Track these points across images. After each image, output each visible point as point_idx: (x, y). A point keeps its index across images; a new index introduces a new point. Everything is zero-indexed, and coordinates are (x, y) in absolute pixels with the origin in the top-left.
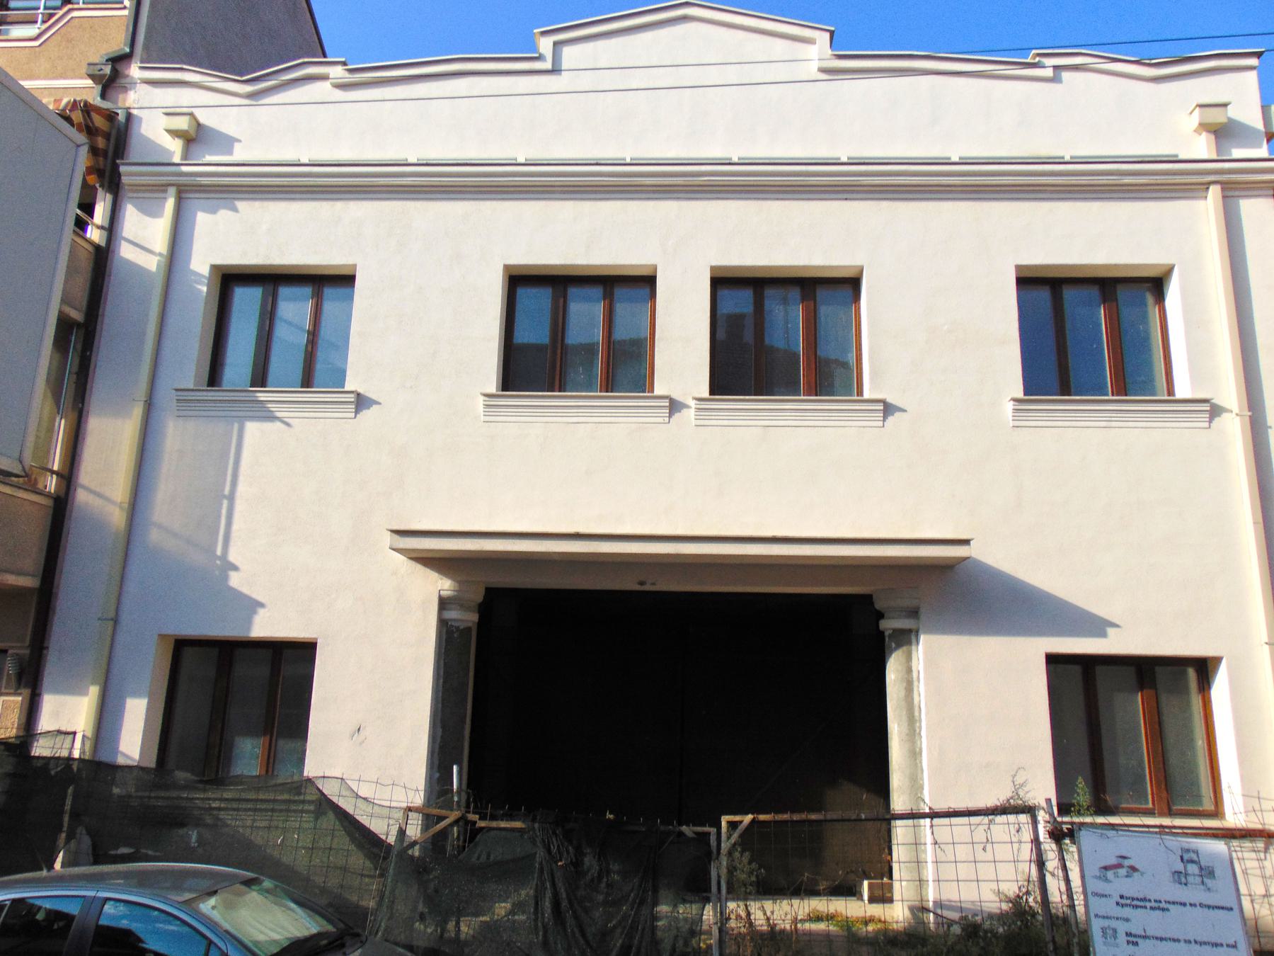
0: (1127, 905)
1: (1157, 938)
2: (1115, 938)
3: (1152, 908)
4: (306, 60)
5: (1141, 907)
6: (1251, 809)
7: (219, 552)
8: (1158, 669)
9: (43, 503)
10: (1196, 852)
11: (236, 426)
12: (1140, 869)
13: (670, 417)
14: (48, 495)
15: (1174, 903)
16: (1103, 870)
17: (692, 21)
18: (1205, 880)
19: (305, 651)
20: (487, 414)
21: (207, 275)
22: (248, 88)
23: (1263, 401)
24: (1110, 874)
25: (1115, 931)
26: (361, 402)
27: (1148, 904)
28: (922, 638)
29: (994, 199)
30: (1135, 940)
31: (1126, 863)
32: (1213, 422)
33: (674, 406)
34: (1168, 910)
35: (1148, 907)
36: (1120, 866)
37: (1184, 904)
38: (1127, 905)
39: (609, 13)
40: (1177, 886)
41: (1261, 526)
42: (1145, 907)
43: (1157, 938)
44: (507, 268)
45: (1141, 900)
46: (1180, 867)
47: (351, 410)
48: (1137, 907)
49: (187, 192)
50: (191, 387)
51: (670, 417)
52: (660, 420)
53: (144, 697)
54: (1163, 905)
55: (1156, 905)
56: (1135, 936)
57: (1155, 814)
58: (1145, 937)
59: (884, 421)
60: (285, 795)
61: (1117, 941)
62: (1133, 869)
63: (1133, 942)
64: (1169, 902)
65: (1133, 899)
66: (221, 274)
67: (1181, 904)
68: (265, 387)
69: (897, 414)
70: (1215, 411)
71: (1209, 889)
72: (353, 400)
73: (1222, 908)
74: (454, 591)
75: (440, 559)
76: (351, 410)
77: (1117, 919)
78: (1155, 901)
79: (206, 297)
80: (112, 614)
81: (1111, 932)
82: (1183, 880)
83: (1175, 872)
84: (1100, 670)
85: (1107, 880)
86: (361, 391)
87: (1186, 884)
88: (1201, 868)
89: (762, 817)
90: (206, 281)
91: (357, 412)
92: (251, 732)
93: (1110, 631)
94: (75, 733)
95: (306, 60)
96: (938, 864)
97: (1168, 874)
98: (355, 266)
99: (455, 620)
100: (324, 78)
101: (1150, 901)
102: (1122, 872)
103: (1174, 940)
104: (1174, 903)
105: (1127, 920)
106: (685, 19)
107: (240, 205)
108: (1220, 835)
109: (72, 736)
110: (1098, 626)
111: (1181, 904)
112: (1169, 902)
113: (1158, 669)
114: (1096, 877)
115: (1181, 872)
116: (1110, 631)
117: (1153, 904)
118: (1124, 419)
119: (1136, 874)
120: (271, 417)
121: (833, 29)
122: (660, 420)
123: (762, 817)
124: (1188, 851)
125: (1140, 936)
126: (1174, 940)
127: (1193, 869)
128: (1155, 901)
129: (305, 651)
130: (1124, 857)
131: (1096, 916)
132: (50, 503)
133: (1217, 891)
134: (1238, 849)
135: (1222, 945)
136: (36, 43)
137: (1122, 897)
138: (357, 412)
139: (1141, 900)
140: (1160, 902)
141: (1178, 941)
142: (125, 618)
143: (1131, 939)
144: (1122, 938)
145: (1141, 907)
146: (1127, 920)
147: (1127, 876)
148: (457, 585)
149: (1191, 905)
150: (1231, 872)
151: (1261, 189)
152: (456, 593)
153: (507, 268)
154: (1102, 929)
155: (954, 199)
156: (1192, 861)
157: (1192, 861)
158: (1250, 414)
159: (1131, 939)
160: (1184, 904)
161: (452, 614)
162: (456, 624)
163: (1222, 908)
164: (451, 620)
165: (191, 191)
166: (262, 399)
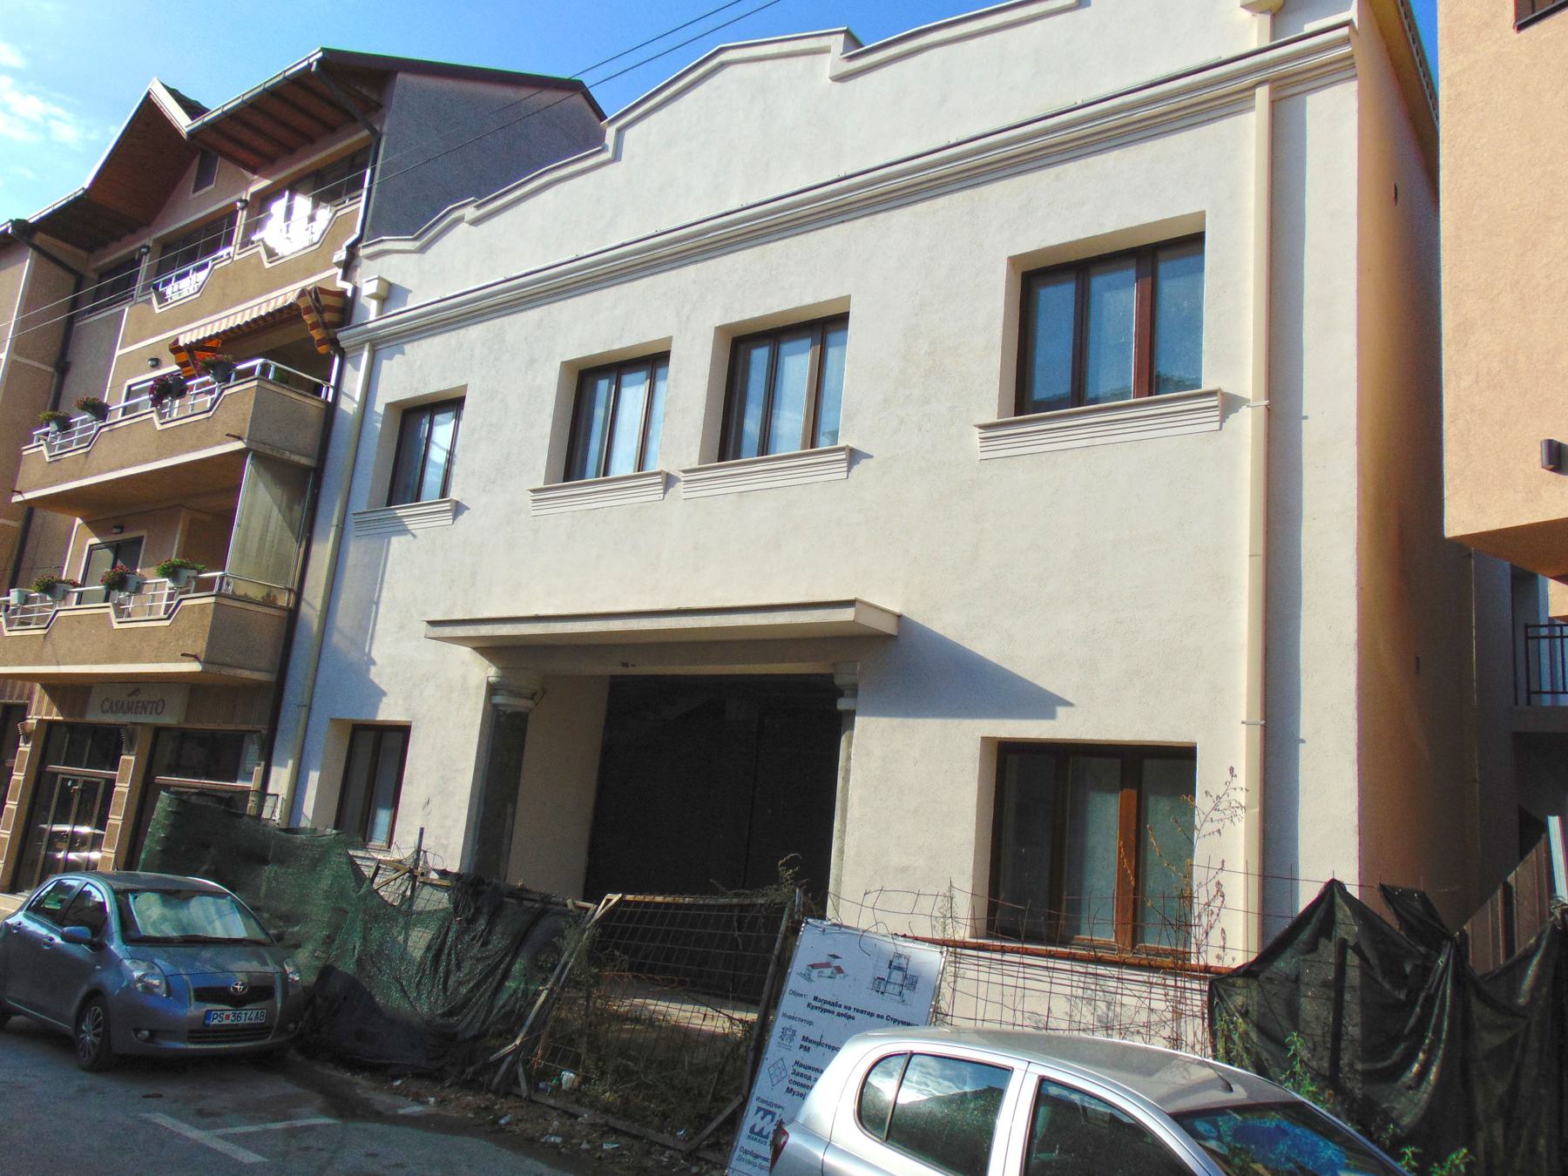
2: (791, 1040)
3: (839, 1014)
4: (451, 207)
5: (829, 1012)
7: (367, 650)
8: (1148, 763)
9: (276, 614)
10: (907, 958)
11: (386, 540)
12: (845, 971)
13: (665, 493)
14: (281, 608)
17: (728, 67)
18: (904, 991)
19: (401, 732)
20: (686, 490)
21: (382, 413)
22: (417, 244)
23: (1301, 380)
24: (815, 972)
25: (794, 1032)
26: (854, 456)
27: (837, 1010)
28: (858, 720)
29: (1049, 164)
31: (836, 963)
32: (1227, 420)
33: (669, 481)
34: (853, 1018)
36: (827, 965)
37: (871, 1015)
39: (794, 33)
40: (874, 992)
41: (1259, 560)
42: (833, 1013)
44: (1014, 261)
46: (884, 975)
47: (842, 469)
48: (826, 1011)
49: (378, 344)
50: (365, 510)
51: (665, 493)
52: (656, 497)
53: (317, 770)
54: (851, 1013)
56: (810, 1041)
57: (1043, 940)
58: (819, 1044)
59: (848, 471)
60: (298, 841)
62: (839, 970)
64: (858, 1011)
65: (825, 1002)
66: (1020, 272)
68: (739, 458)
69: (864, 462)
70: (1230, 404)
72: (449, 508)
74: (497, 677)
75: (506, 648)
76: (842, 469)
78: (846, 1007)
79: (381, 433)
80: (306, 702)
84: (1148, 764)
85: (809, 979)
86: (852, 445)
88: (905, 977)
89: (629, 897)
90: (381, 419)
91: (454, 518)
92: (384, 807)
93: (1061, 711)
94: (277, 795)
95: (451, 207)
97: (870, 980)
98: (1202, 215)
99: (504, 705)
100: (460, 220)
102: (828, 972)
105: (810, 1023)
106: (723, 65)
107: (407, 348)
109: (275, 797)
110: (1045, 704)
112: (858, 1011)
113: (1148, 763)
114: (800, 974)
115: (883, 979)
116: (1061, 711)
117: (842, 1010)
118: (1027, 444)
119: (838, 976)
120: (405, 531)
121: (845, 28)
122: (656, 497)
123: (629, 897)
124: (900, 956)
125: (814, 1042)
127: (897, 976)
128: (846, 1007)
129: (401, 732)
130: (835, 957)
131: (784, 1015)
132: (285, 614)
133: (910, 1005)
134: (1021, 975)
136: (199, 295)
137: (815, 998)
138: (454, 518)
140: (850, 1008)
142: (315, 706)
144: (798, 1041)
145: (829, 1012)
146: (810, 1023)
147: (830, 977)
148: (500, 672)
151: (1338, 71)
152: (499, 679)
153: (1014, 261)
155: (978, 184)
156: (899, 968)
157: (899, 968)
158: (1266, 402)
160: (871, 1015)
161: (498, 699)
162: (503, 709)
164: (500, 704)
165: (382, 343)
166: (399, 515)
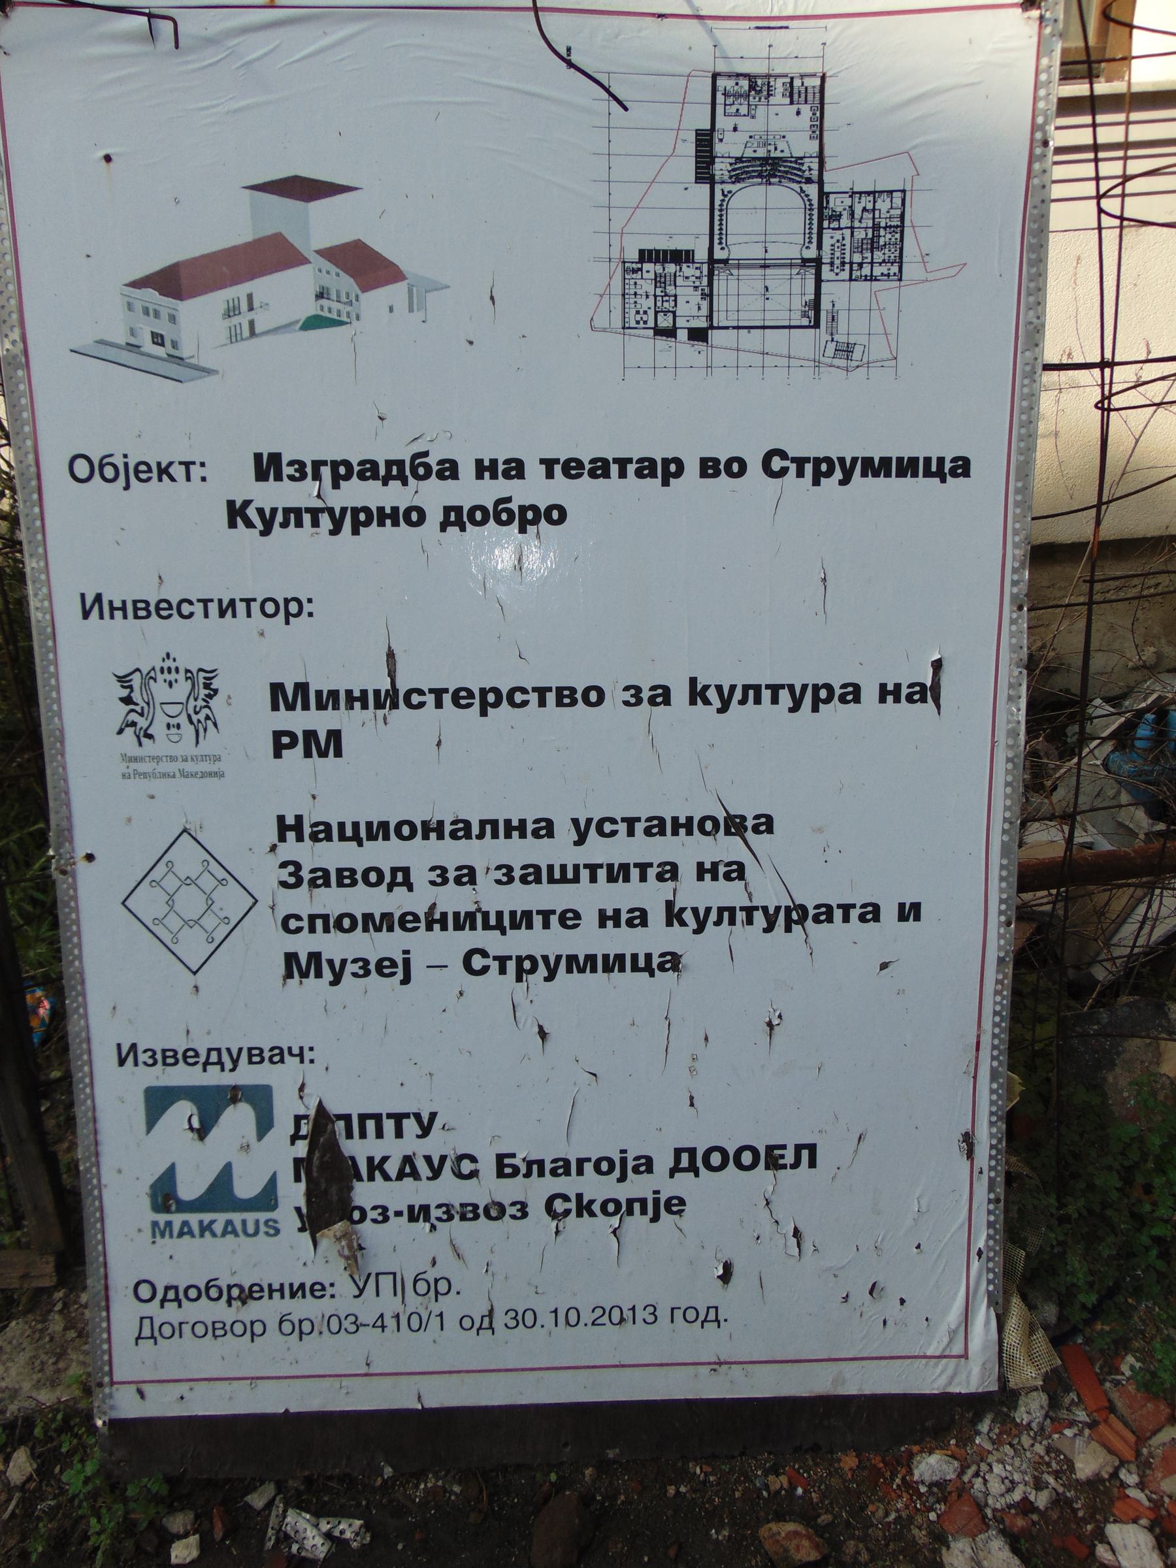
0: (294, 516)
1: (461, 697)
3: (454, 518)
5: (389, 516)
6: (350, 1390)
15: (600, 469)
16: (151, 295)
18: (835, 292)
30: (321, 721)
35: (535, 471)
37: (671, 470)
38: (294, 516)
42: (415, 516)
43: (461, 697)
45: (395, 472)
48: (361, 518)
55: (488, 492)
56: (329, 700)
61: (212, 742)
63: (310, 735)
64: (572, 468)
65: (341, 472)
67: (647, 468)
71: (846, 351)
73: (908, 467)
77: (227, 608)
78: (486, 469)
81: (183, 688)
82: (690, 310)
83: (646, 256)
87: (698, 335)
96: (1119, 199)
101: (449, 470)
103: (566, 697)
104: (600, 469)
108: (1028, 316)
111: (647, 468)
112: (572, 468)
115: (680, 257)
126: (566, 697)
135: (853, 693)
139: (395, 472)
141: (594, 696)
143: (298, 721)
145: (389, 516)
149: (709, 467)
150: (1165, 229)
154: (124, 680)
159: (298, 721)
163: (908, 467)
